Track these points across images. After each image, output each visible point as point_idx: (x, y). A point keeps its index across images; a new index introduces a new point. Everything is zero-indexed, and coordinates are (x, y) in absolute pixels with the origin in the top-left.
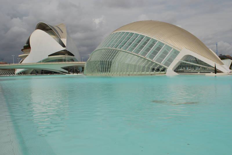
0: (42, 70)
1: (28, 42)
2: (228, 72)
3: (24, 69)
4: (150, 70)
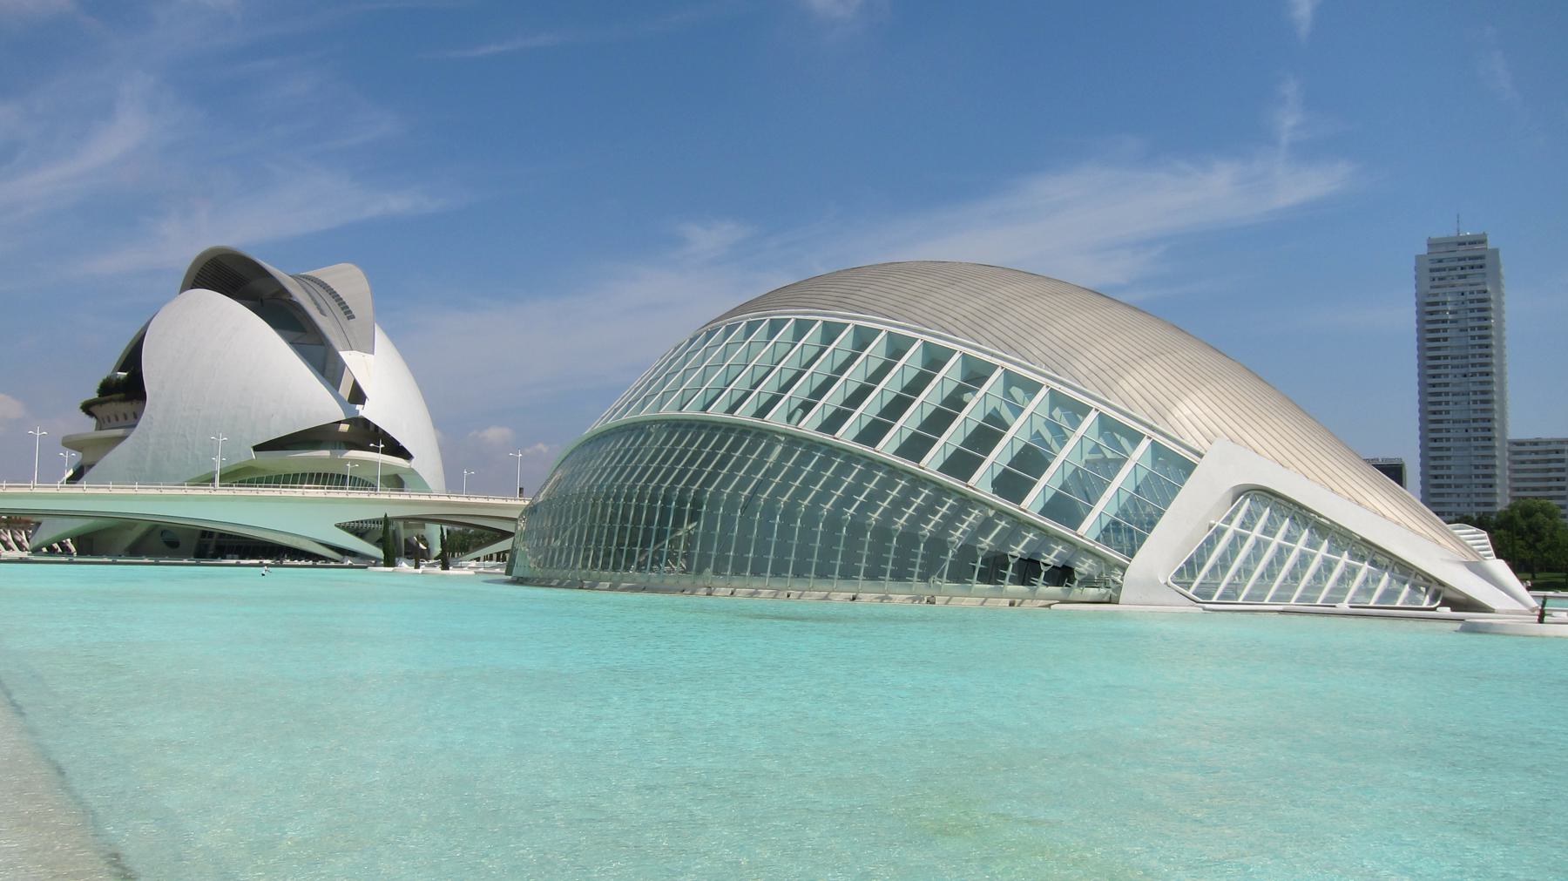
1: (132, 360)
3: (91, 521)
4: (1009, 572)
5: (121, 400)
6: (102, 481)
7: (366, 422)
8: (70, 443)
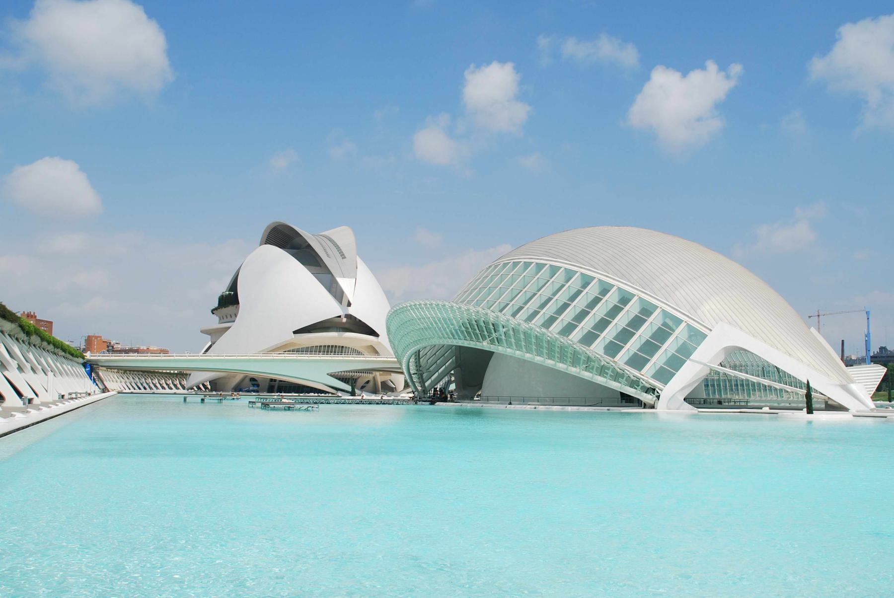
0: (272, 380)
1: (234, 286)
2: (863, 408)
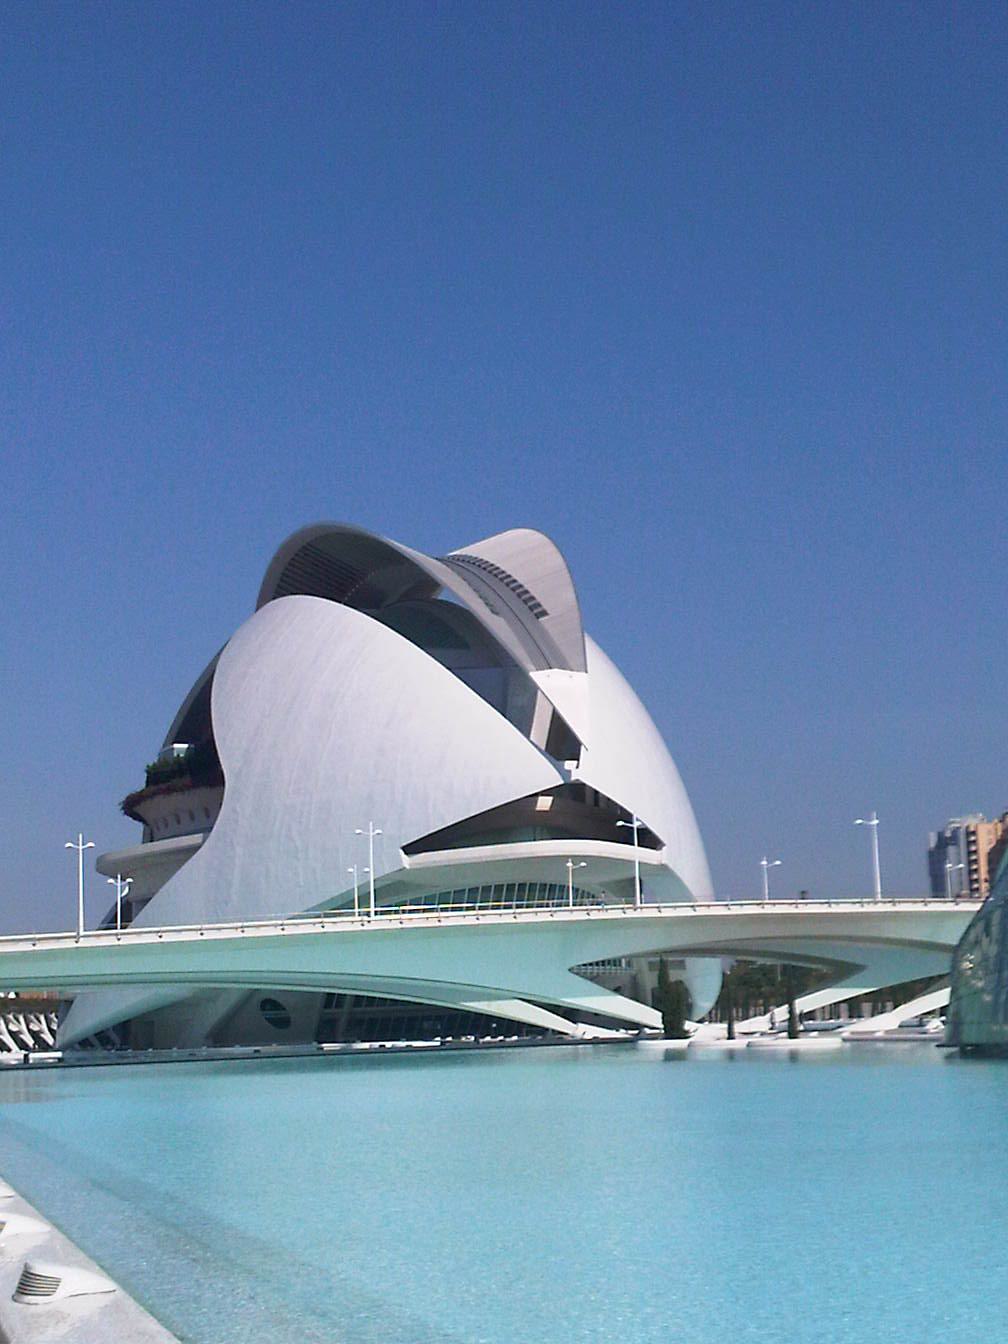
1: (195, 722)
5: (188, 788)
6: (175, 919)
7: (580, 787)
8: (106, 867)
